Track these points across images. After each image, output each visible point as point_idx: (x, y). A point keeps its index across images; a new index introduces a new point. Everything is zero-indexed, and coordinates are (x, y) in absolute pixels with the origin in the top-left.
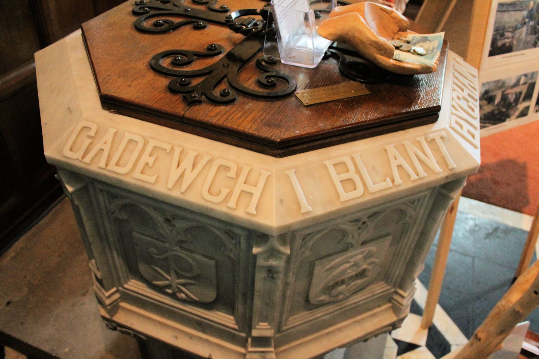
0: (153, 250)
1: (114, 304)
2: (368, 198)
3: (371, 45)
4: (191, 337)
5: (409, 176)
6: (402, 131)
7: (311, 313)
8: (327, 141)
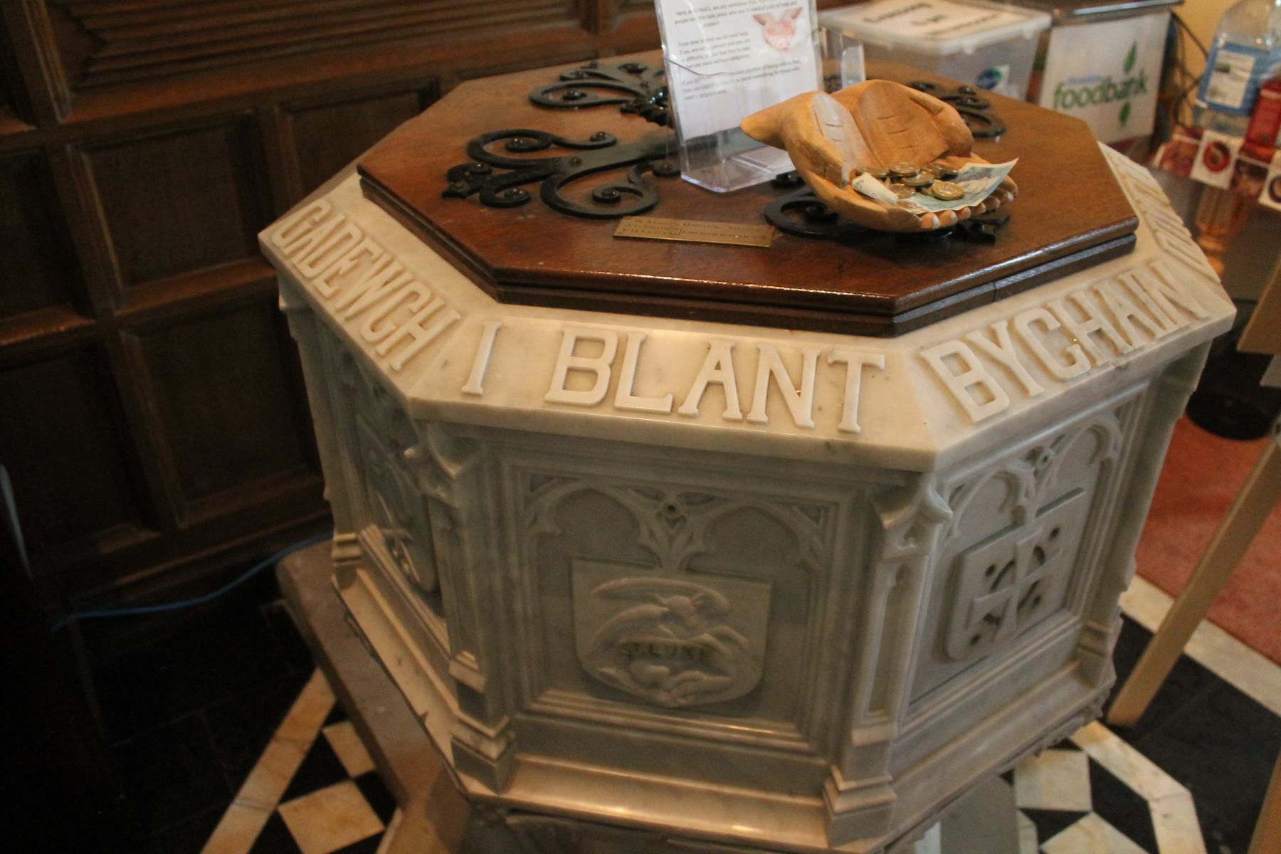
0: (373, 455)
1: (347, 563)
2: (605, 414)
3: (800, 149)
4: (418, 670)
5: (725, 407)
6: (787, 331)
7: (597, 703)
8: (600, 297)
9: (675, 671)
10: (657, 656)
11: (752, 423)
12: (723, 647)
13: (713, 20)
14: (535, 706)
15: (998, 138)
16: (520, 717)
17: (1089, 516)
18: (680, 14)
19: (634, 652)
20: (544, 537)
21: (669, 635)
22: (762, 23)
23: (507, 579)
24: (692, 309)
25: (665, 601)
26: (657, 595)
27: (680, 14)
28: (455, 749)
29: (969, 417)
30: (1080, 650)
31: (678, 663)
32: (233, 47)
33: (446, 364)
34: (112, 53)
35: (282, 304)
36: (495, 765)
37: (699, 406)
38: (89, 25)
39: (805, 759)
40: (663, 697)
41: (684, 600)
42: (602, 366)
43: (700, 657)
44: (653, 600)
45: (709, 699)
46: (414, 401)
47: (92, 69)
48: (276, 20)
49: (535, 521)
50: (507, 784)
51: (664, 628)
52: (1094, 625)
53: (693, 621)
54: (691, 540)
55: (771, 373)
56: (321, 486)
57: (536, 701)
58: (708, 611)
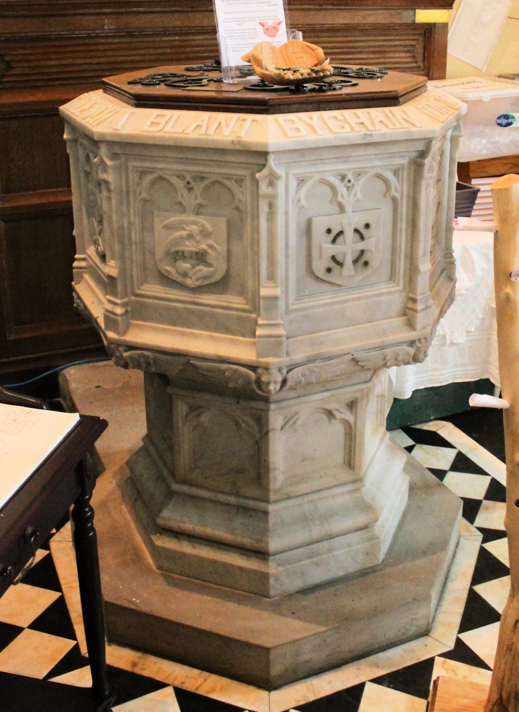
2: (161, 134)
9: (193, 267)
10: (185, 257)
11: (208, 135)
12: (210, 251)
13: (240, 23)
14: (138, 292)
15: (379, 79)
16: (133, 298)
17: (393, 228)
18: (226, 19)
19: (177, 256)
20: (145, 201)
21: (189, 246)
22: (263, 26)
23: (130, 223)
24: (200, 106)
25: (187, 229)
26: (184, 226)
27: (226, 19)
28: (106, 318)
29: (287, 135)
30: (407, 310)
31: (194, 262)
32: (74, 75)
33: (111, 122)
34: (15, 73)
35: (65, 136)
36: (119, 318)
37: (192, 131)
38: (7, 58)
39: (246, 314)
40: (189, 282)
41: (195, 227)
42: (163, 123)
43: (200, 257)
44: (183, 229)
45: (208, 282)
46: (97, 132)
47: (5, 80)
48: (97, 63)
49: (140, 193)
50: (124, 333)
51: (188, 243)
52: (411, 295)
53: (198, 238)
54: (196, 198)
55: (220, 123)
56: (72, 228)
57: (139, 289)
58: (206, 234)
